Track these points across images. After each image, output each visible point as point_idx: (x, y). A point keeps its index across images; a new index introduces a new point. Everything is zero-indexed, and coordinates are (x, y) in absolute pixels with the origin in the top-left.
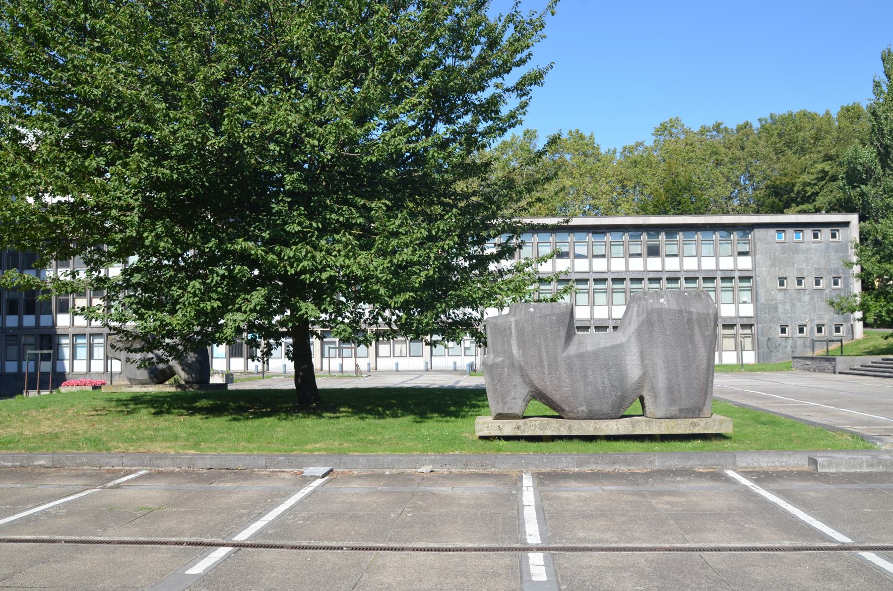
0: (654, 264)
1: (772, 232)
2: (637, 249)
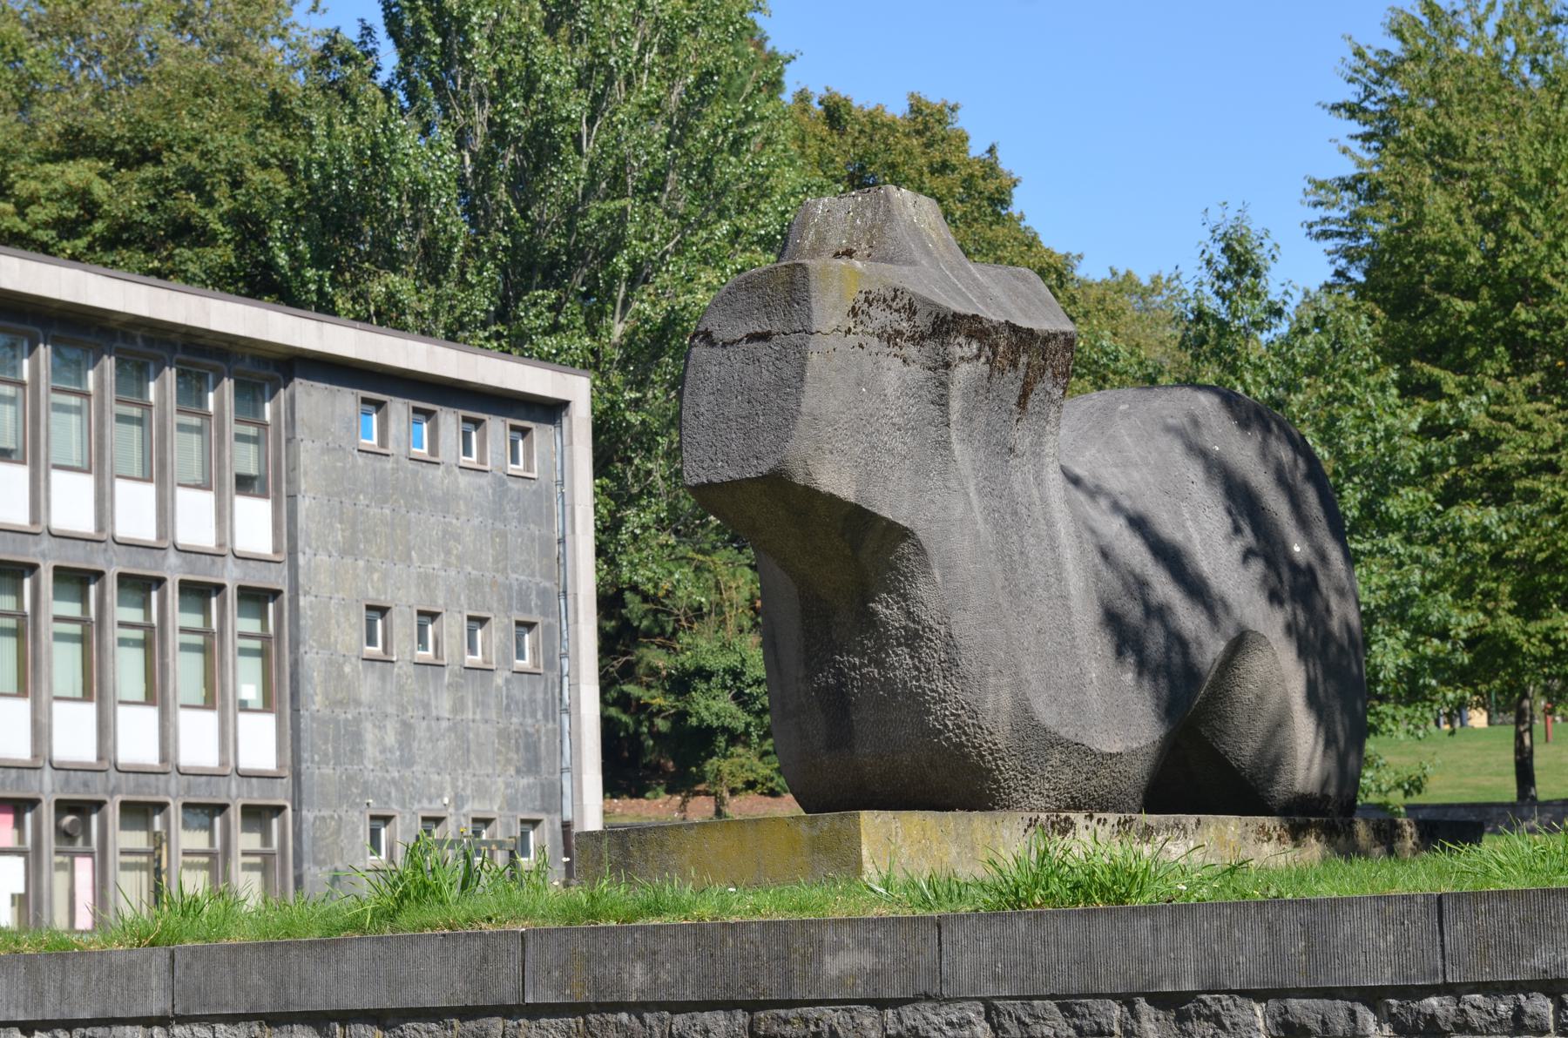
1: (348, 399)
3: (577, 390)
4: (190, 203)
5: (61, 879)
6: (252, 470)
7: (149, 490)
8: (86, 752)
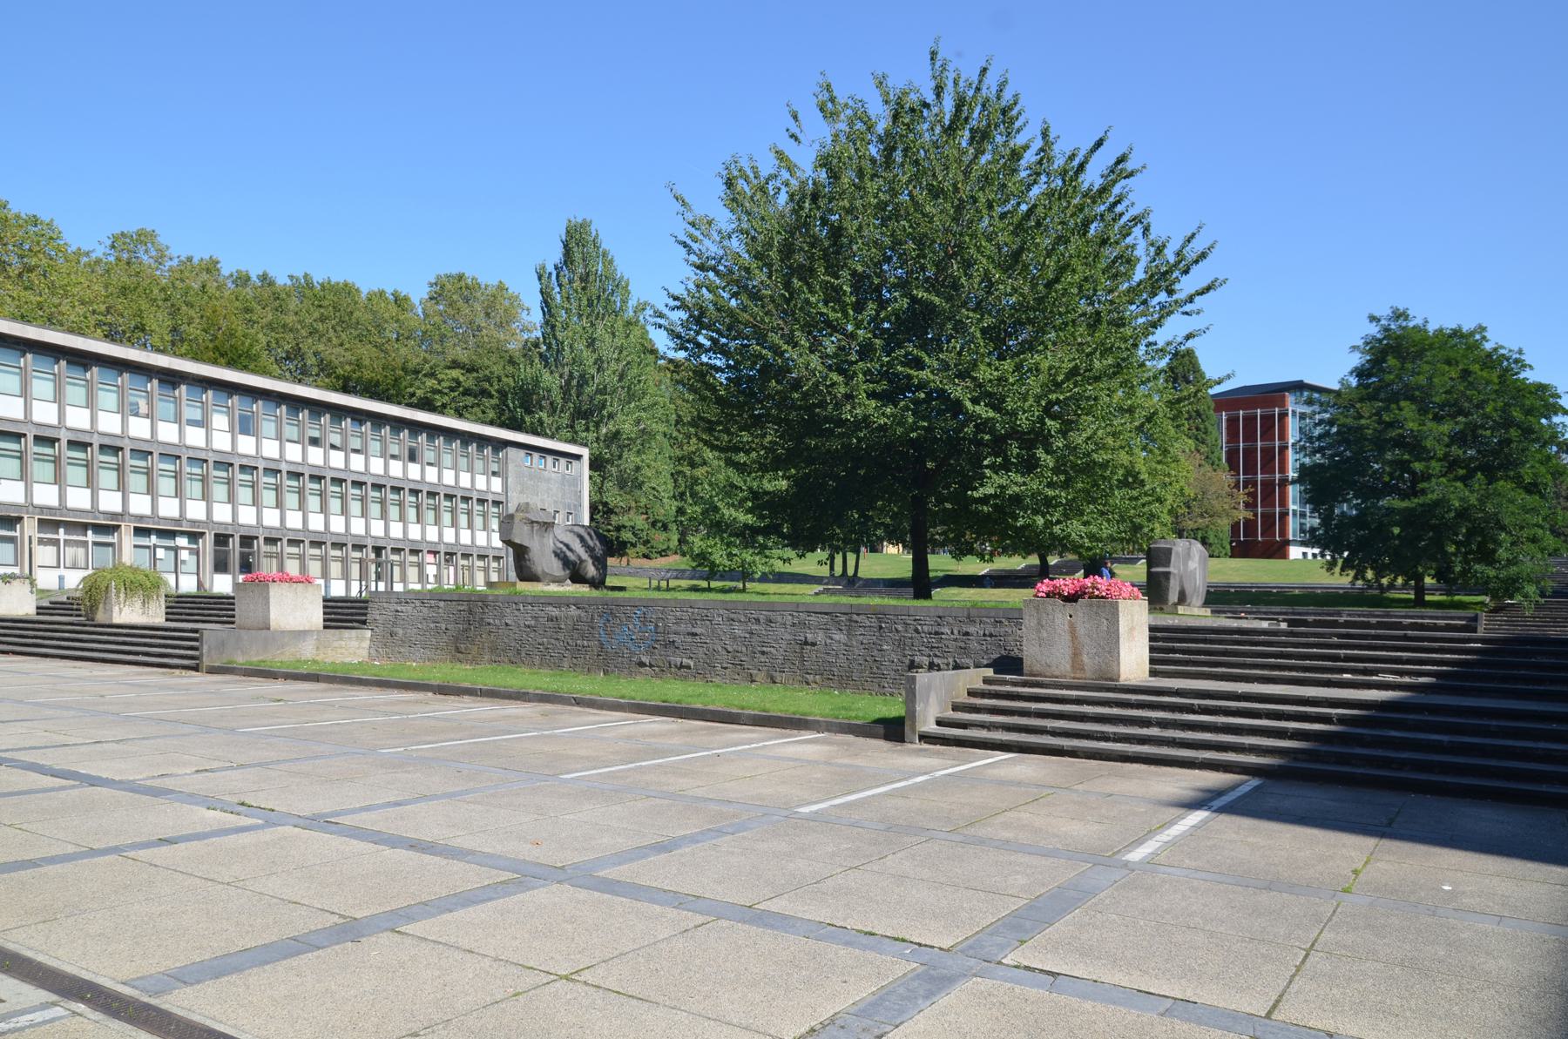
0: (414, 471)
1: (522, 453)
2: (394, 449)
3: (585, 452)
4: (486, 385)
5: (446, 571)
6: (496, 470)
7: (469, 474)
8: (452, 540)
